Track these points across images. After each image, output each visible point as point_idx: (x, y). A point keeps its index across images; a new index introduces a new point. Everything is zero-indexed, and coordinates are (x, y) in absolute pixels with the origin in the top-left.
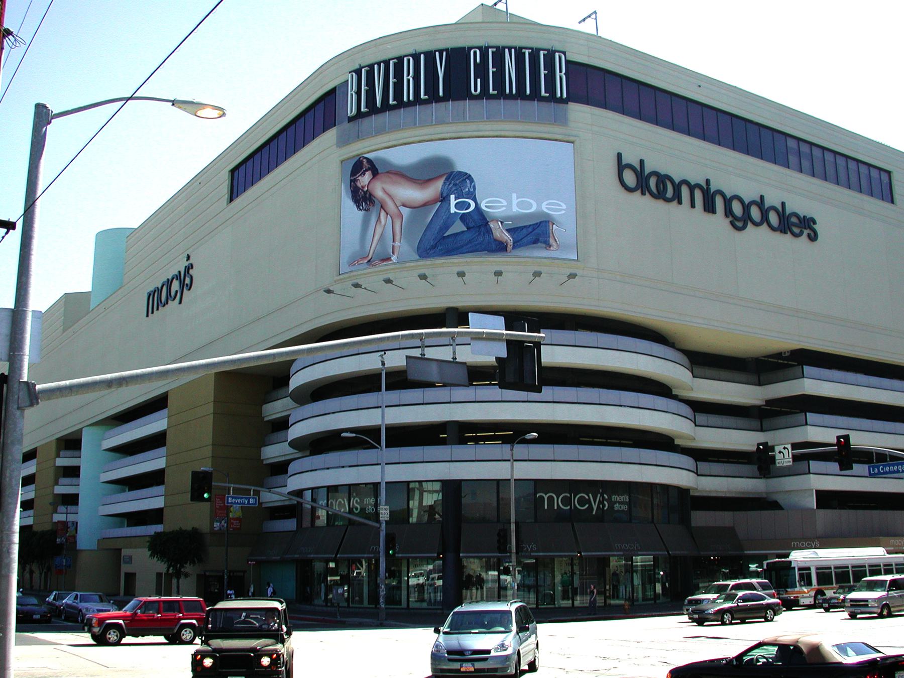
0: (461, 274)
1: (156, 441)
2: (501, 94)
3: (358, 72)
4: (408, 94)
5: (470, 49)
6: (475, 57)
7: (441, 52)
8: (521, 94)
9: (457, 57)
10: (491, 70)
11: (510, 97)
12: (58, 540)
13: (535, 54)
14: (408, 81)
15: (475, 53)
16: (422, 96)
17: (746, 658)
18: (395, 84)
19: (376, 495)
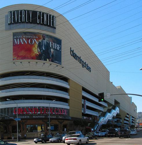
0: (29, 62)
1: (65, 100)
2: (43, 24)
3: (11, 12)
4: (23, 20)
5: (37, 12)
6: (38, 14)
7: (16, 11)
8: (47, 25)
9: (34, 13)
10: (41, 18)
11: (45, 25)
12: (95, 121)
13: (50, 15)
14: (23, 17)
15: (38, 13)
16: (19, 21)
17: (129, 96)
18: (20, 17)
19: (16, 112)
